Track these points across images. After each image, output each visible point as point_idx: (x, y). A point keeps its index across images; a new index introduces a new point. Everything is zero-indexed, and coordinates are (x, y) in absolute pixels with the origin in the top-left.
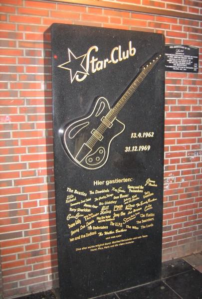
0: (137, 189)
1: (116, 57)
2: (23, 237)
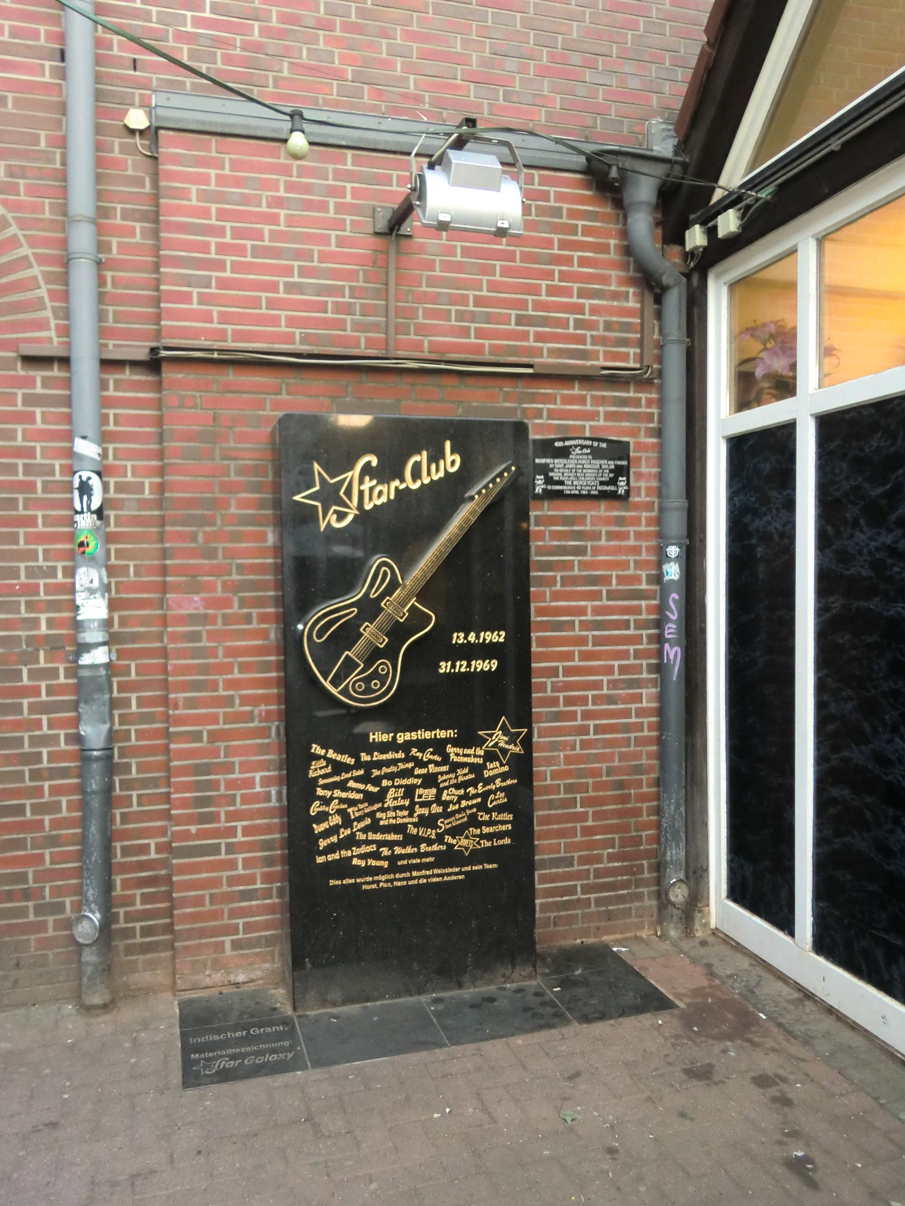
0: (469, 756)
1: (416, 475)
2: (223, 856)
